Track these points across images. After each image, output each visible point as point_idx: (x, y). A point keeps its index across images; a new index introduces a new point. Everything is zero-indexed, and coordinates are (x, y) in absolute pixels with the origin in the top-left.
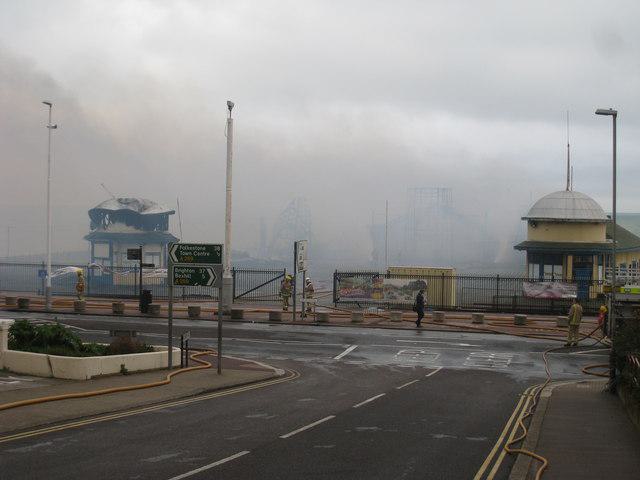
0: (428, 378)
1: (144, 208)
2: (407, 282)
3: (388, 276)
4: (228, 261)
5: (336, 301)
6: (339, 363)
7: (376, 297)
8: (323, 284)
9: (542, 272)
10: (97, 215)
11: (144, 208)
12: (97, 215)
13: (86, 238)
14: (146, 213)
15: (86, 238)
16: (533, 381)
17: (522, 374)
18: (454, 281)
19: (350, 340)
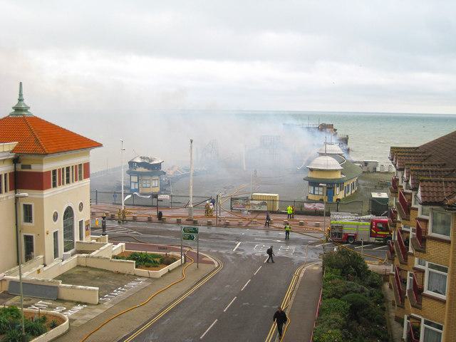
0: (130, 194)
1: (151, 161)
2: (259, 202)
3: (252, 200)
4: (163, 168)
5: (232, 209)
6: (235, 254)
7: (247, 208)
8: (225, 203)
9: (314, 190)
10: (131, 163)
11: (151, 161)
12: (131, 163)
13: (13, 108)
14: (152, 163)
15: (13, 108)
16: (301, 264)
17: (297, 259)
18: (278, 202)
19: (238, 238)
